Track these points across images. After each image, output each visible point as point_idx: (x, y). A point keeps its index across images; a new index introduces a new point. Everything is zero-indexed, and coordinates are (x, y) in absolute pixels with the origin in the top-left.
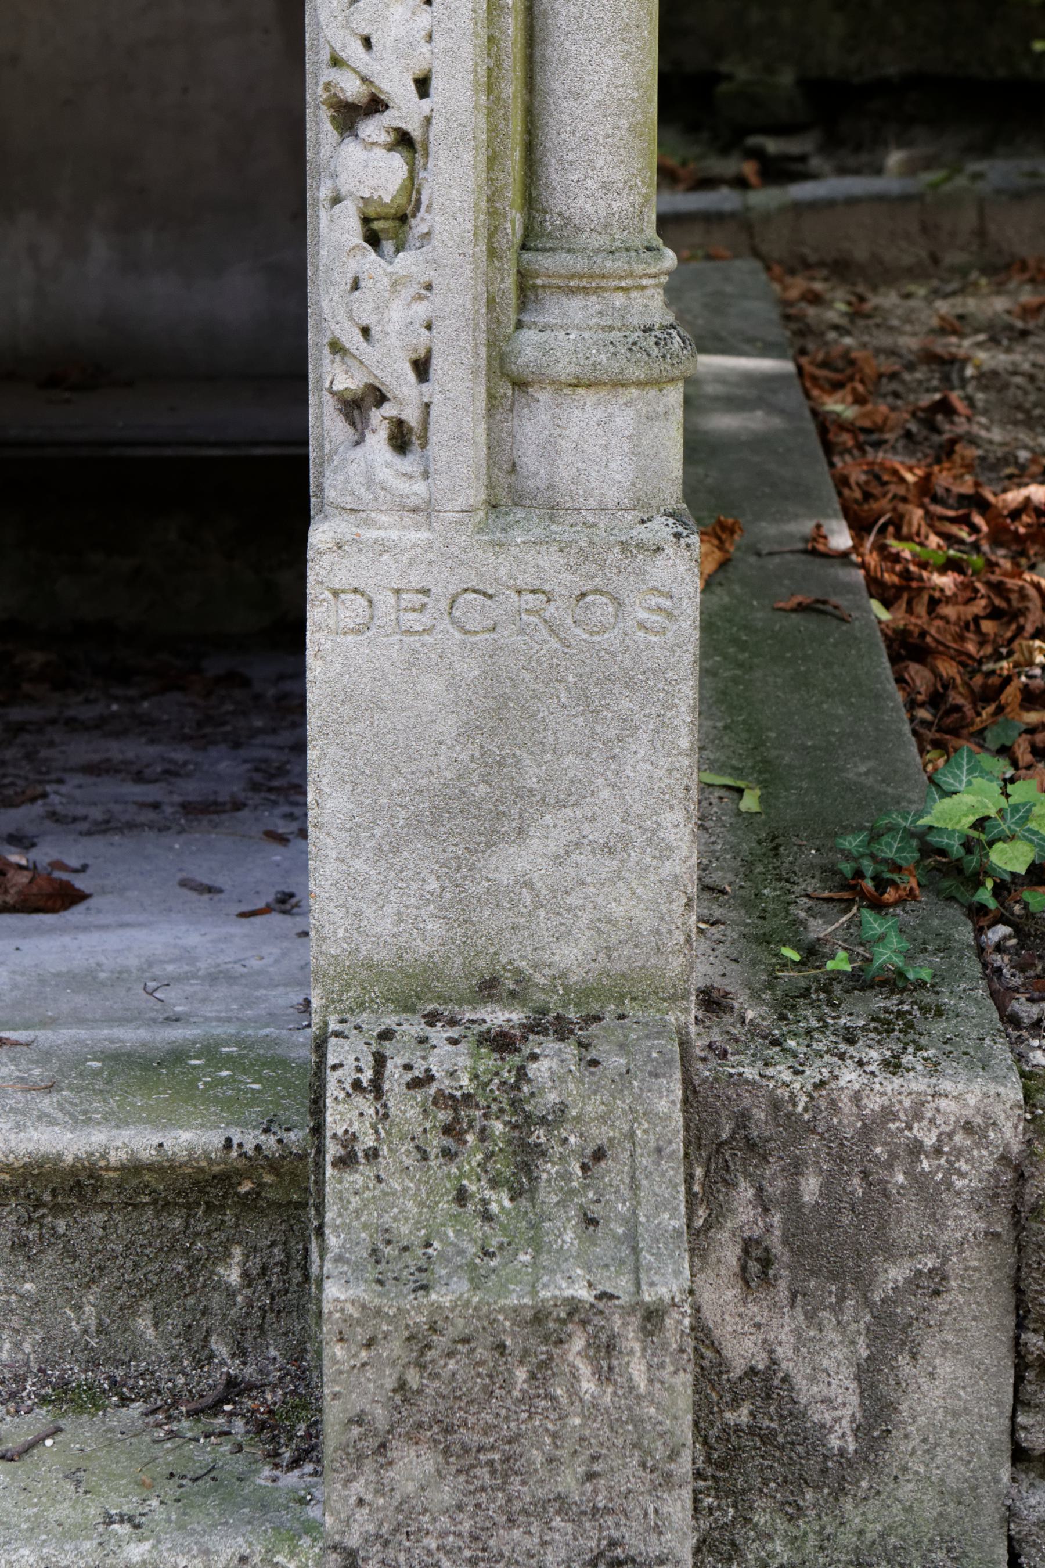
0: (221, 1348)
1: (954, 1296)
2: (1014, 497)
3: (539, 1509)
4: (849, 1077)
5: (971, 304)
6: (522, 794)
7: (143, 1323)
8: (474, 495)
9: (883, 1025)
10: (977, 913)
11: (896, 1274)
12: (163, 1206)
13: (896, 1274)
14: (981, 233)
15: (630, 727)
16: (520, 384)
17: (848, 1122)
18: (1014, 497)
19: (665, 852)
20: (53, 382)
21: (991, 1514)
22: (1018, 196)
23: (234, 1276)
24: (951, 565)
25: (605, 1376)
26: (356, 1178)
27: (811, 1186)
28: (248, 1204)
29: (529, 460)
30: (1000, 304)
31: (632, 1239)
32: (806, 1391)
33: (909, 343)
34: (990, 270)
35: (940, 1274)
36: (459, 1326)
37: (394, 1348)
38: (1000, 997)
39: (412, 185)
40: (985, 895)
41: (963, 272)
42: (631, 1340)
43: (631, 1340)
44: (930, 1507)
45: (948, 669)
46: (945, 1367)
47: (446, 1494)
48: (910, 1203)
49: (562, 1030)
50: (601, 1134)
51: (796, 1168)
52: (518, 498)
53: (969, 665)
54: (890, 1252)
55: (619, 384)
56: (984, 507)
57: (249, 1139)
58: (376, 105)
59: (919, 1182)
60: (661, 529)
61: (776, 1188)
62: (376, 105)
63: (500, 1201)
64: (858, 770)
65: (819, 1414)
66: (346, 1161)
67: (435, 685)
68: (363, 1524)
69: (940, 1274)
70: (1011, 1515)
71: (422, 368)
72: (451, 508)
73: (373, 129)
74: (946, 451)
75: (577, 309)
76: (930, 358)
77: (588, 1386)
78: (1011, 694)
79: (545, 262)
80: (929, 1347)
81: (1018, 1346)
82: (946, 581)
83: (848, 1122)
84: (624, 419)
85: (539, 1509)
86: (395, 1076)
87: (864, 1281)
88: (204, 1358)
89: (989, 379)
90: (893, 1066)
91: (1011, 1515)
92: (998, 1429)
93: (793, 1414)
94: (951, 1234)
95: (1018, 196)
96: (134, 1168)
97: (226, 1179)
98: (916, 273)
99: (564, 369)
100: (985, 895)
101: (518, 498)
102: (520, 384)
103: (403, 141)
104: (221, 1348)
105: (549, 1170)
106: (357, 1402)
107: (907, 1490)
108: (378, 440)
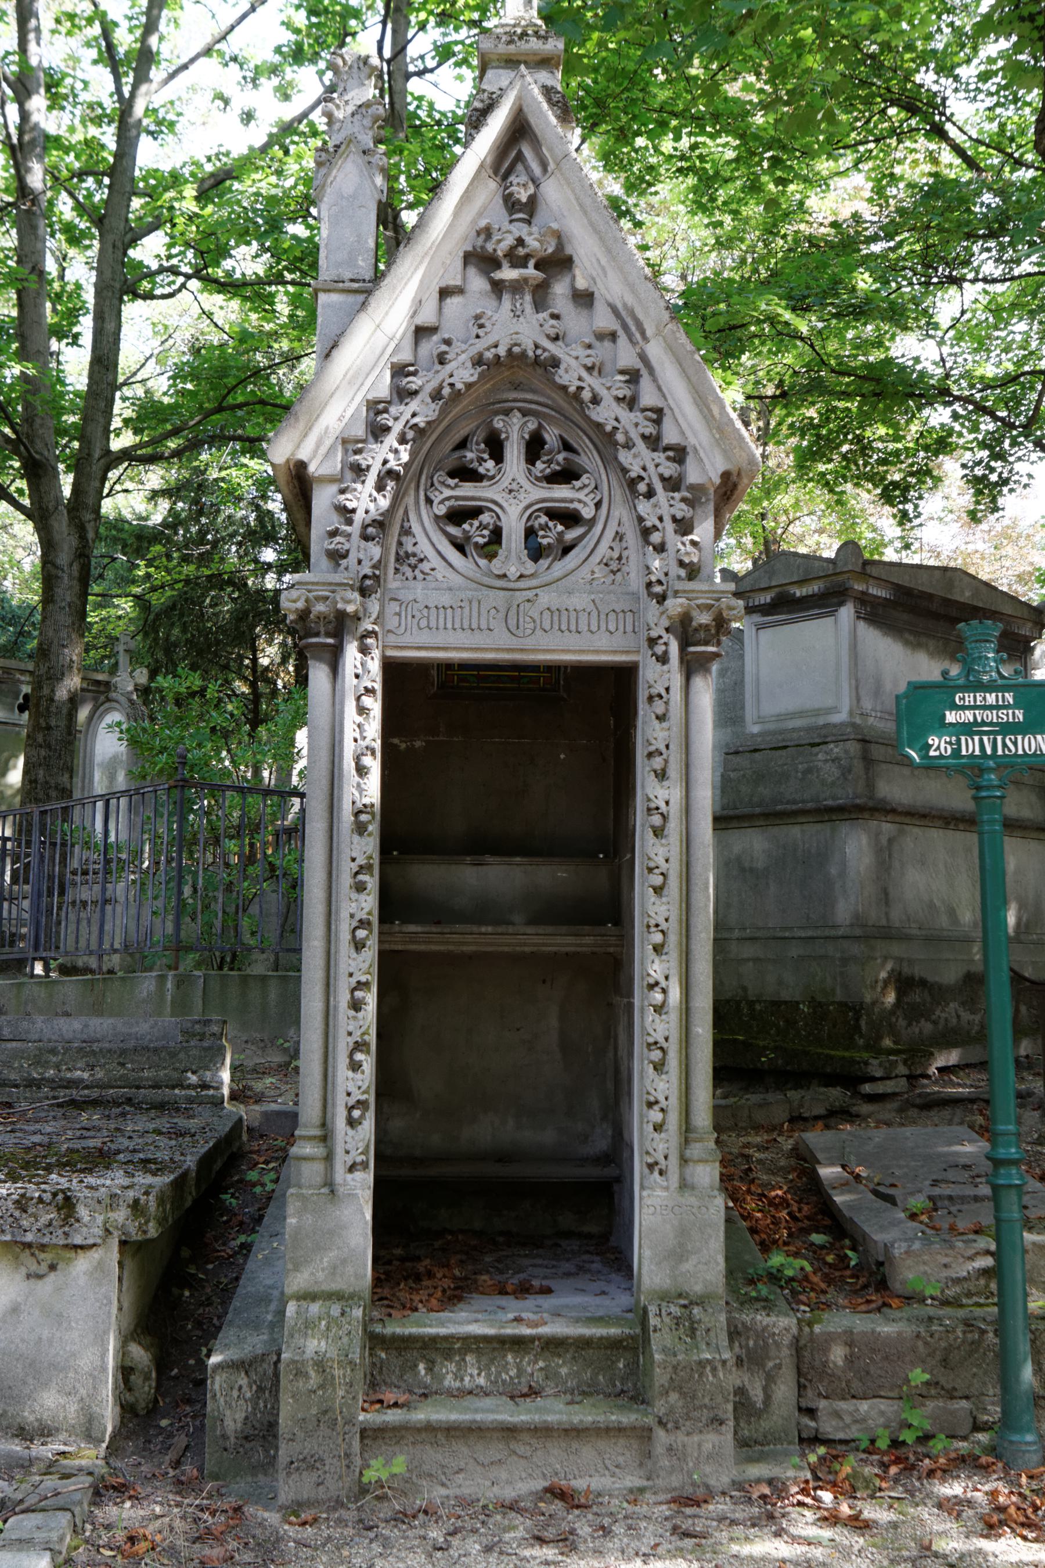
0: (618, 1384)
1: (784, 1369)
2: (773, 1194)
3: (701, 1407)
4: (759, 1317)
5: (750, 1139)
6: (688, 1251)
7: (601, 1377)
8: (676, 1185)
9: (764, 1308)
10: (781, 1287)
11: (770, 1364)
12: (606, 1348)
13: (770, 1364)
14: (750, 1117)
15: (710, 1236)
16: (686, 1161)
17: (759, 1328)
18: (773, 1194)
19: (718, 1264)
20: (500, 1160)
21: (794, 1424)
22: (760, 1106)
23: (621, 1365)
24: (760, 1211)
25: (714, 1376)
26: (658, 1334)
27: (751, 1343)
28: (625, 1348)
29: (688, 1178)
30: (759, 1139)
31: (718, 1347)
32: (752, 1393)
33: (735, 1151)
34: (753, 1128)
35: (780, 1364)
36: (683, 1364)
37: (669, 1369)
38: (789, 1304)
39: (664, 1119)
40: (783, 1283)
41: (745, 1129)
42: (720, 1368)
43: (720, 1368)
44: (780, 1422)
45: (764, 1236)
46: (782, 1387)
47: (680, 1404)
48: (773, 1347)
49: (697, 1304)
50: (709, 1325)
51: (748, 1338)
52: (685, 1186)
53: (769, 1235)
54: (769, 1359)
55: (707, 1161)
56: (765, 1196)
57: (627, 1331)
58: (657, 1102)
59: (775, 1342)
60: (716, 1193)
61: (743, 1343)
62: (657, 1102)
63: (688, 1340)
64: (747, 1257)
65: (755, 1399)
66: (655, 1331)
67: (668, 1226)
68: (663, 1411)
69: (780, 1364)
70: (798, 1423)
71: (666, 1158)
72: (672, 1188)
73: (656, 1107)
74: (753, 1181)
75: (698, 1145)
76: (743, 1155)
77: (711, 1378)
78: (780, 1242)
79: (691, 1135)
80: (779, 1382)
81: (799, 1382)
82: (759, 1215)
83: (759, 1328)
84: (708, 1169)
85: (701, 1407)
86: (664, 1313)
87: (763, 1366)
88: (614, 1386)
89: (760, 1161)
90: (768, 1315)
91: (798, 1423)
92: (794, 1402)
93: (748, 1398)
94: (783, 1354)
95: (760, 1106)
96: (601, 1338)
97: (621, 1341)
98: (730, 1129)
99: (696, 1158)
100: (783, 1283)
101: (685, 1186)
102: (686, 1161)
103: (662, 1110)
104: (618, 1384)
105: (698, 1333)
106: (662, 1382)
107: (775, 1418)
108: (656, 1173)
